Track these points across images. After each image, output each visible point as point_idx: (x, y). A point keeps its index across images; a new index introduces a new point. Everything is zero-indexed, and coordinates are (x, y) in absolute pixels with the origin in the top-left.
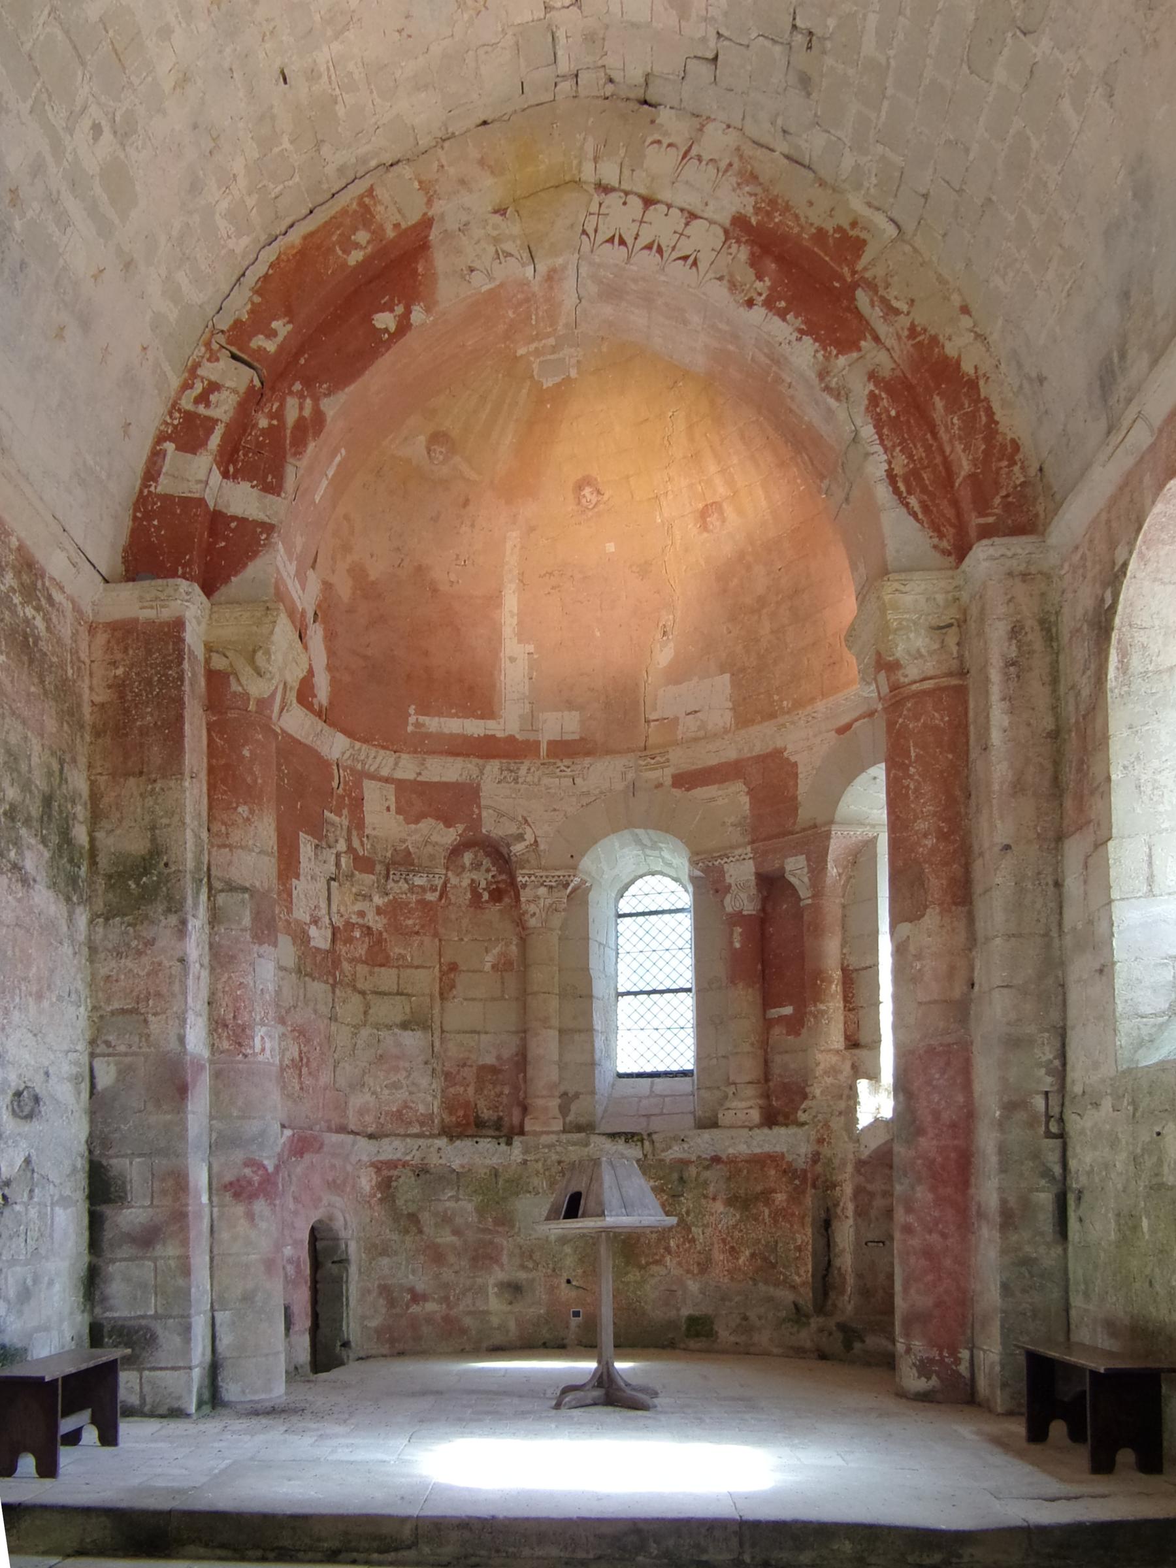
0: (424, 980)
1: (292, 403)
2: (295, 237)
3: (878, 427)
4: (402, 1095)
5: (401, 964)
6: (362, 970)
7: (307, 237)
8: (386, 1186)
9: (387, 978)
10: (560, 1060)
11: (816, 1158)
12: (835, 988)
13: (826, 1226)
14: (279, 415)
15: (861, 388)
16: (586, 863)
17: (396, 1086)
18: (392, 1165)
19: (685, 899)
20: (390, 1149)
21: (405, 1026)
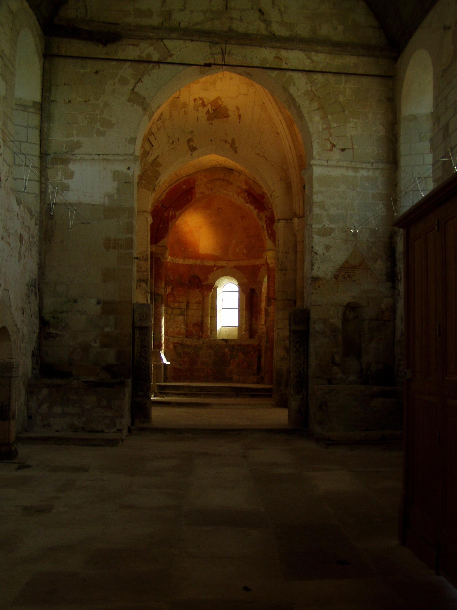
0: (184, 306)
1: (171, 212)
2: (173, 186)
3: (267, 225)
4: (178, 329)
5: (179, 302)
6: (172, 303)
7: (175, 186)
8: (175, 347)
9: (176, 305)
10: (145, 154)
11: (258, 345)
12: (263, 313)
13: (259, 358)
14: (168, 214)
15: (264, 219)
16: (217, 282)
17: (177, 327)
18: (176, 343)
19: (237, 289)
20: (176, 340)
21: (179, 315)
